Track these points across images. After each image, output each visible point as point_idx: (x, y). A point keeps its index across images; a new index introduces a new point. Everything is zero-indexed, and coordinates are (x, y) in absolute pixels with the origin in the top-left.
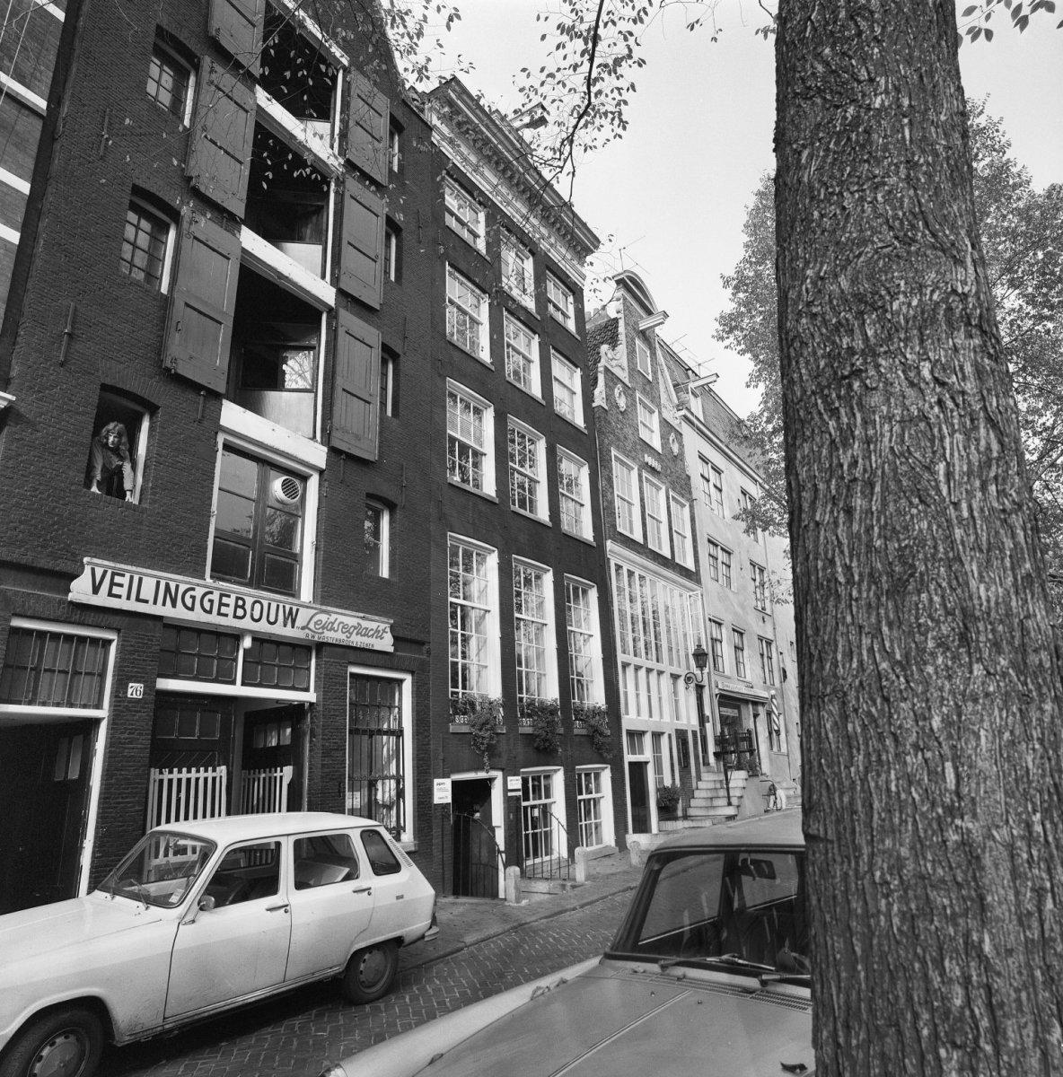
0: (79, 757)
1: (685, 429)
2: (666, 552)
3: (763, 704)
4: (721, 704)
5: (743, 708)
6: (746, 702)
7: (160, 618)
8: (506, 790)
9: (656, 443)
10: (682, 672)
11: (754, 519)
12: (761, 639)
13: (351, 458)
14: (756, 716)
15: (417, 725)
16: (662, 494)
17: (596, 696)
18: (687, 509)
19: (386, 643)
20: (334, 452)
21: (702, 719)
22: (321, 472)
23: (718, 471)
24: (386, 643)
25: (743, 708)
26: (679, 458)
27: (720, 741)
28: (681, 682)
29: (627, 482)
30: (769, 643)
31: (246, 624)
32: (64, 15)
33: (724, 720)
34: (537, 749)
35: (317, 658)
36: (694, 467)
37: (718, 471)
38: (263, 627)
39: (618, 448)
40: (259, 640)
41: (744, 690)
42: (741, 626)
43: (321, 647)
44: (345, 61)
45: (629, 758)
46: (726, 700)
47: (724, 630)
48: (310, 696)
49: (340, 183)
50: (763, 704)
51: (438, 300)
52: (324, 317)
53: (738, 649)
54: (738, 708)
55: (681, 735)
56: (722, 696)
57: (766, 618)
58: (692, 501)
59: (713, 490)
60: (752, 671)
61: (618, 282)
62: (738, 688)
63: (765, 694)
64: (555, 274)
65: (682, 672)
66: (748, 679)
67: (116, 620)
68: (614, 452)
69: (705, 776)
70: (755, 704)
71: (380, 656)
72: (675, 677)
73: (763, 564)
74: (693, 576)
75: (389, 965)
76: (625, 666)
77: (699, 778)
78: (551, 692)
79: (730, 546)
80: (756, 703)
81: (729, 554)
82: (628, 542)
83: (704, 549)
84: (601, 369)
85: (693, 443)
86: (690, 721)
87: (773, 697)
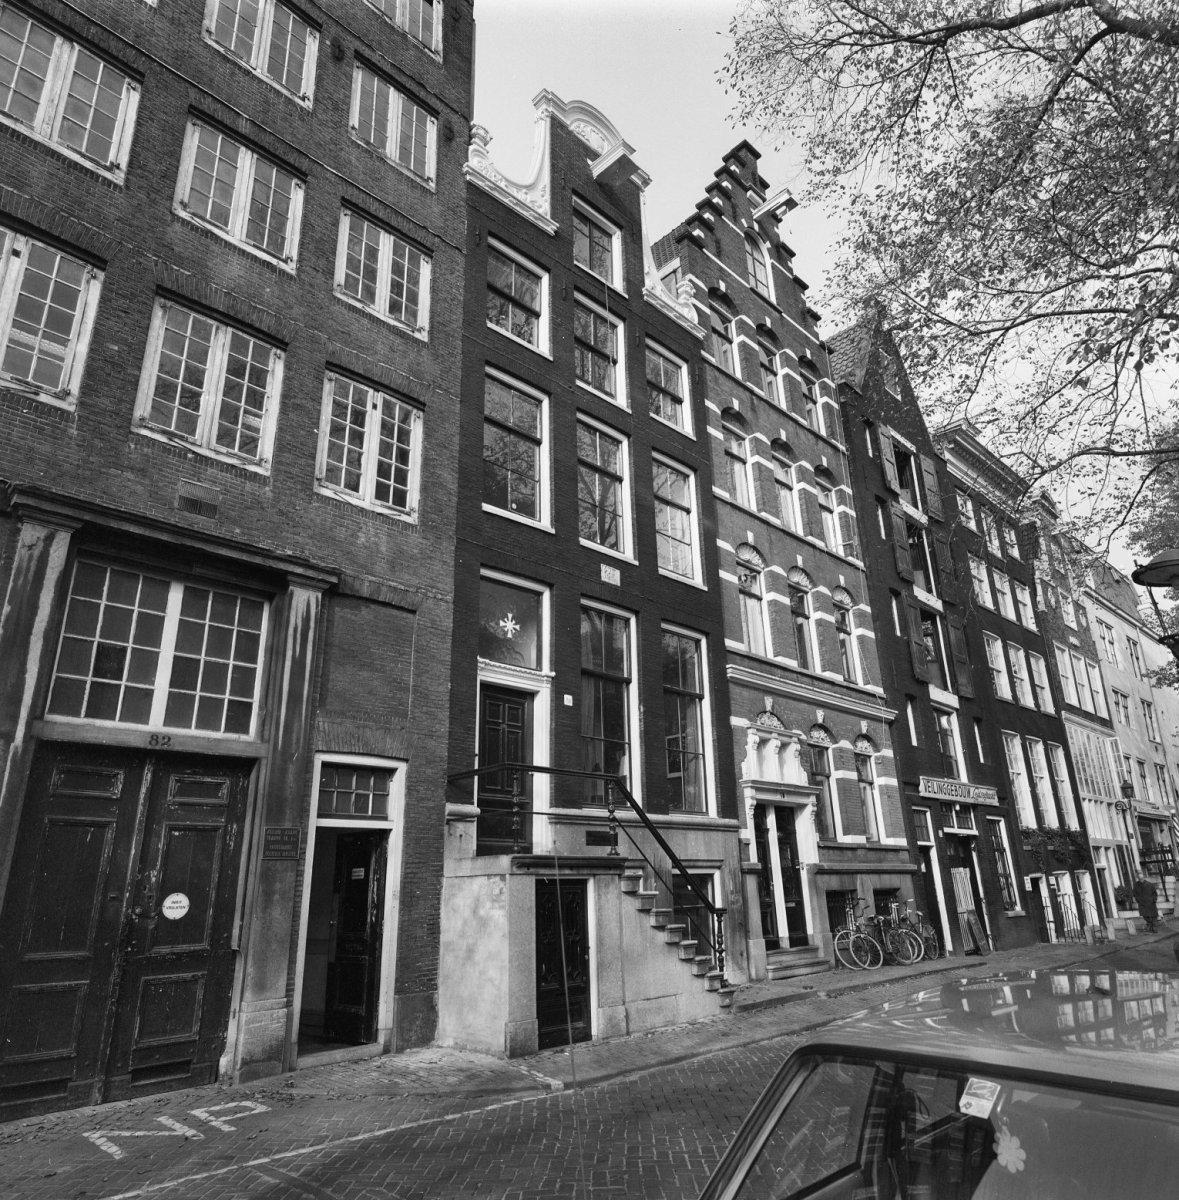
0: (805, 1074)
6: (1154, 820)
9: (1074, 626)
12: (1156, 765)
15: (556, 495)
16: (1082, 661)
21: (1129, 836)
23: (1109, 627)
28: (1113, 807)
29: (1063, 659)
30: (1162, 767)
32: (932, 696)
35: (248, 1161)
37: (1109, 627)
41: (1153, 811)
44: (913, 449)
49: (917, 457)
52: (912, 459)
58: (1098, 662)
62: (1148, 810)
63: (1167, 813)
66: (1152, 800)
67: (929, 803)
68: (1055, 643)
72: (1109, 805)
73: (1150, 700)
79: (1125, 691)
83: (1112, 698)
87: (1173, 815)
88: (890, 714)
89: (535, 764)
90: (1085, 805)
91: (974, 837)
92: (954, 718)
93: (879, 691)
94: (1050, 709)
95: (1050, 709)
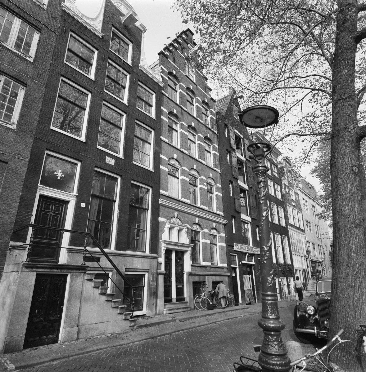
1: (299, 193)
2: (298, 226)
3: (320, 263)
4: (312, 263)
5: (316, 264)
6: (317, 262)
7: (240, 251)
8: (278, 281)
10: (303, 255)
11: (321, 216)
13: (254, 219)
14: (319, 266)
16: (296, 211)
17: (289, 262)
18: (301, 214)
19: (107, 158)
20: (252, 218)
21: (308, 267)
22: (251, 222)
23: (306, 201)
24: (107, 158)
25: (316, 264)
26: (298, 201)
27: (312, 272)
28: (303, 257)
29: (290, 210)
30: (320, 246)
31: (248, 252)
33: (313, 267)
34: (282, 273)
36: (302, 202)
37: (306, 201)
38: (249, 252)
39: (288, 203)
40: (249, 254)
41: (316, 259)
42: (314, 242)
43: (254, 254)
45: (296, 276)
46: (313, 262)
47: (315, 246)
48: (254, 263)
49: (246, 163)
50: (320, 263)
51: (135, 126)
53: (314, 248)
54: (315, 264)
55: (304, 270)
56: (312, 261)
57: (320, 239)
59: (305, 206)
60: (317, 254)
61: (284, 159)
63: (321, 260)
64: (274, 165)
65: (303, 255)
67: (238, 252)
69: (310, 281)
70: (319, 263)
71: (143, 182)
72: (302, 256)
74: (303, 231)
75: (99, 184)
76: (293, 254)
77: (309, 281)
78: (282, 261)
79: (310, 221)
80: (319, 262)
81: (310, 223)
82: (291, 225)
83: (305, 223)
84: (283, 184)
85: (301, 195)
86: (305, 267)
87: (323, 261)
88: (225, 222)
89: (65, 229)
90: (294, 256)
91: (254, 265)
92: (249, 225)
93: (222, 214)
94: (284, 224)
95: (284, 224)
